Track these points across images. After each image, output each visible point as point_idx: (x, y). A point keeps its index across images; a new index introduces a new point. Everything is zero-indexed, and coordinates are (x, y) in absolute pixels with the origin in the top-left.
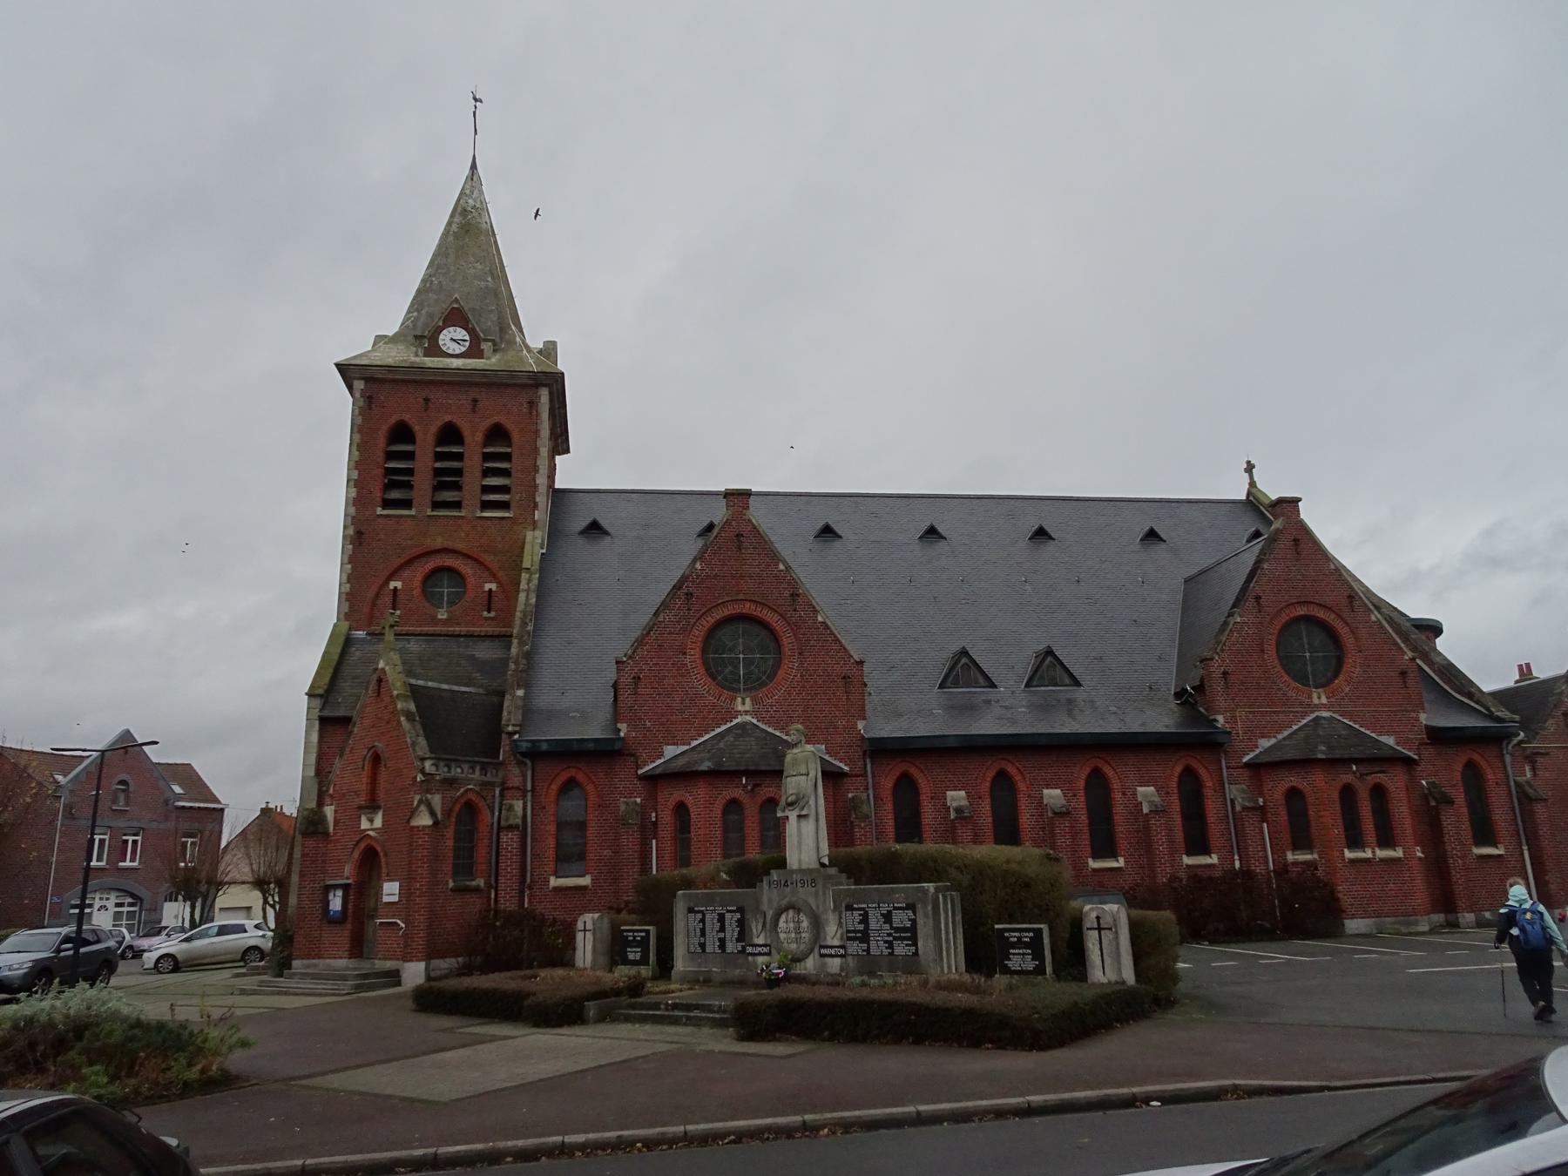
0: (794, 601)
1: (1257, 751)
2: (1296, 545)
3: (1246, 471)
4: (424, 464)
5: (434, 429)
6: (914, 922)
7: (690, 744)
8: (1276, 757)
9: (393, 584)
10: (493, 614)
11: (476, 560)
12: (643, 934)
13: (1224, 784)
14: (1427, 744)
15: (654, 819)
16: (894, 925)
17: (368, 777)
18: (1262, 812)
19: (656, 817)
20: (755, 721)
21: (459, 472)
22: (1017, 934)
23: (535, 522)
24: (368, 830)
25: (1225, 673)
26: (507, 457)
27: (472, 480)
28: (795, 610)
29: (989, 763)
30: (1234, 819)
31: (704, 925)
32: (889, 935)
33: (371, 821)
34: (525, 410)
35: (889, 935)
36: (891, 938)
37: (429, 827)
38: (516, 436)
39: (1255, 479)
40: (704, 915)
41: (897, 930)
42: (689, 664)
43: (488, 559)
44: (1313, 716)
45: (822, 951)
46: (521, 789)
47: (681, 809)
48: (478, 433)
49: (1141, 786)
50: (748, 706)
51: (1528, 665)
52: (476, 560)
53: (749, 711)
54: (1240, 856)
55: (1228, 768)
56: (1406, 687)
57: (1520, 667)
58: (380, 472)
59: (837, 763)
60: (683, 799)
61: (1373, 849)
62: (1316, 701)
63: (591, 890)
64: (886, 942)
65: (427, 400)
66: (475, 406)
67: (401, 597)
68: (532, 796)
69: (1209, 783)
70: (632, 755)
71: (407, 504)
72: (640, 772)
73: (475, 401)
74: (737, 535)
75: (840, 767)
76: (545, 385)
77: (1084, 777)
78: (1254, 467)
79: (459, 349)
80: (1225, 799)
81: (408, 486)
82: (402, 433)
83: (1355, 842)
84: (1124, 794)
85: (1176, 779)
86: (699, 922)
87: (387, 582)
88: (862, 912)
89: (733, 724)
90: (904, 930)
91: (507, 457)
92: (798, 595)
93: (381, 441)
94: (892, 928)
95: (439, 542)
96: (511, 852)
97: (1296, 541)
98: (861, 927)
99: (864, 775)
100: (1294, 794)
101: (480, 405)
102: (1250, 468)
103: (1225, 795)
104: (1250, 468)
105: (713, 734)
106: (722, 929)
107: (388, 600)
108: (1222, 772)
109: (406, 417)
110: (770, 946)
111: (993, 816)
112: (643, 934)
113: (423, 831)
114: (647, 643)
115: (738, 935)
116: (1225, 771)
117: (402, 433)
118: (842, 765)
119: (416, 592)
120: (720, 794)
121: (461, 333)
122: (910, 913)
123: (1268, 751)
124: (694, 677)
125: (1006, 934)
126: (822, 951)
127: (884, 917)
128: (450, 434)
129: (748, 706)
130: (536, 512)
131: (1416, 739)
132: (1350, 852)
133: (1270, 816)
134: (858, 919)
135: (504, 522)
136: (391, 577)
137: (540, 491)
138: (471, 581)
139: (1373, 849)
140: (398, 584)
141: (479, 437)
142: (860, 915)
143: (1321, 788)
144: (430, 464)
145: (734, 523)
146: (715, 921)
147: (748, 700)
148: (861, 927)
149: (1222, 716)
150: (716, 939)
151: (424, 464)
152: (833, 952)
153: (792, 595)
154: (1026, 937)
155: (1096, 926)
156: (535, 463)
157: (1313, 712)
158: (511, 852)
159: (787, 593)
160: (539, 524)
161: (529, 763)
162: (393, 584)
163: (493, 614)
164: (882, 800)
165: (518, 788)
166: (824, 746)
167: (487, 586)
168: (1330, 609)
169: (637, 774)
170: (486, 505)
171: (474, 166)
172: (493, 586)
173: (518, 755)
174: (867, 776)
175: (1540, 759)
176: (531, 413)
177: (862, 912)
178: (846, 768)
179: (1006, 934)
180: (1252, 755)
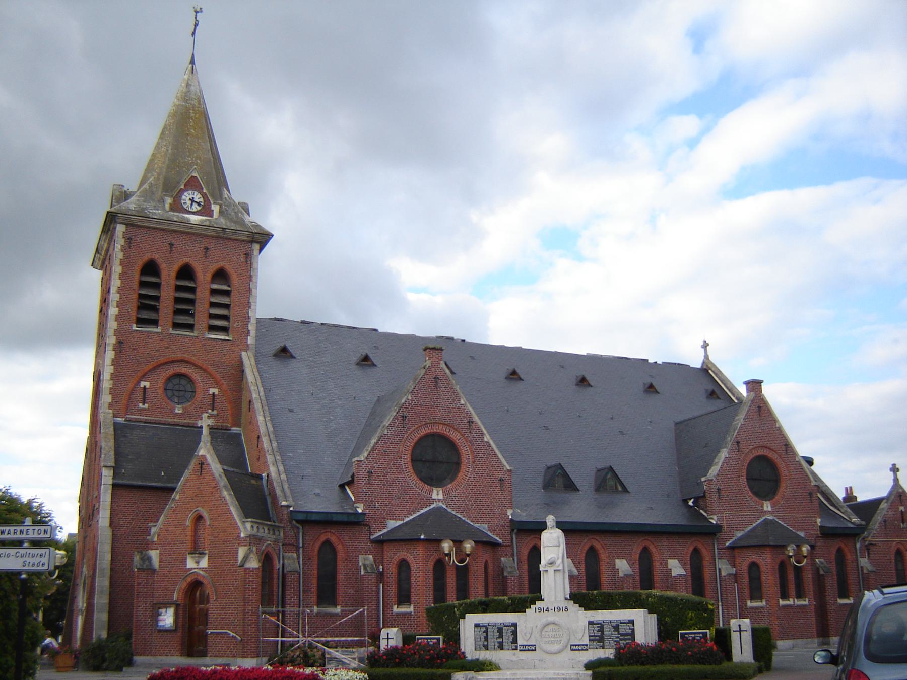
0: (470, 426)
1: (734, 539)
2: (759, 410)
3: (702, 347)
4: (167, 294)
5: (176, 268)
6: (633, 630)
7: (403, 520)
8: (742, 543)
9: (143, 384)
10: (215, 412)
11: (205, 370)
12: (435, 641)
13: (715, 558)
14: (821, 537)
15: (381, 570)
16: (620, 632)
17: (192, 532)
18: (381, 576)
19: (383, 569)
20: (444, 506)
21: (192, 302)
22: (693, 635)
23: (248, 345)
24: (195, 569)
25: (719, 489)
26: (227, 293)
27: (202, 308)
28: (470, 432)
29: (585, 541)
30: (720, 581)
31: (487, 634)
32: (618, 637)
33: (198, 562)
34: (242, 260)
35: (618, 637)
36: (618, 639)
37: (256, 569)
38: (234, 278)
39: (708, 353)
40: (487, 629)
41: (622, 635)
42: (403, 465)
43: (211, 369)
44: (764, 518)
45: (572, 648)
46: (294, 545)
47: (403, 565)
48: (207, 275)
49: (670, 559)
50: (441, 497)
51: (851, 488)
52: (205, 370)
53: (441, 500)
54: (722, 603)
55: (718, 549)
56: (812, 502)
57: (846, 489)
58: (135, 296)
59: (494, 537)
60: (405, 557)
61: (794, 599)
62: (765, 509)
63: (340, 616)
64: (615, 641)
65: (171, 245)
66: (206, 253)
67: (149, 393)
68: (303, 550)
69: (707, 557)
70: (368, 525)
71: (155, 323)
72: (372, 537)
73: (207, 249)
74: (435, 378)
75: (496, 540)
76: (258, 242)
77: (639, 552)
78: (708, 345)
79: (195, 208)
80: (716, 568)
81: (155, 309)
82: (151, 268)
83: (785, 596)
84: (661, 563)
85: (689, 555)
86: (484, 632)
87: (138, 383)
88: (599, 625)
89: (431, 507)
90: (627, 634)
91: (227, 293)
92: (472, 422)
93: (136, 276)
94: (619, 633)
95: (179, 355)
96: (293, 588)
97: (759, 407)
98: (599, 634)
99: (511, 545)
100: (754, 566)
101: (209, 252)
102: (705, 345)
103: (715, 566)
104: (705, 345)
105: (418, 514)
106: (501, 636)
107: (139, 395)
108: (714, 551)
109: (156, 256)
110: (535, 645)
111: (586, 576)
112: (435, 641)
113: (252, 571)
114: (377, 449)
115: (513, 639)
116: (716, 550)
117: (151, 268)
118: (497, 539)
119: (160, 391)
120: (432, 555)
121: (197, 197)
122: (631, 625)
123: (741, 539)
124: (406, 474)
125: (687, 636)
126: (572, 648)
127: (614, 628)
128: (186, 272)
129: (441, 497)
130: (249, 337)
131: (814, 534)
132: (783, 601)
133: (386, 579)
134: (597, 629)
135: (225, 343)
136: (143, 377)
137: (252, 322)
138: (200, 386)
139: (794, 599)
140: (147, 384)
141: (209, 277)
142: (598, 627)
143: (766, 561)
144: (172, 294)
145: (433, 369)
146: (496, 631)
147: (441, 492)
148: (599, 634)
149: (716, 516)
150: (496, 643)
151: (167, 294)
152: (580, 648)
153: (469, 422)
154: (698, 637)
155: (738, 629)
156: (249, 301)
157: (764, 515)
158: (293, 588)
159: (465, 421)
160: (251, 346)
161: (301, 527)
162: (143, 384)
163: (146, 406)
164: (521, 562)
165: (293, 545)
166: (487, 526)
167: (212, 391)
168: (775, 451)
169: (370, 539)
170: (212, 328)
171: (193, 55)
172: (216, 391)
173: (294, 522)
174: (513, 547)
175: (871, 548)
176: (246, 263)
177: (599, 625)
178: (500, 541)
179: (687, 636)
180: (730, 542)
